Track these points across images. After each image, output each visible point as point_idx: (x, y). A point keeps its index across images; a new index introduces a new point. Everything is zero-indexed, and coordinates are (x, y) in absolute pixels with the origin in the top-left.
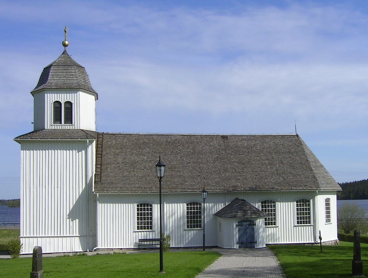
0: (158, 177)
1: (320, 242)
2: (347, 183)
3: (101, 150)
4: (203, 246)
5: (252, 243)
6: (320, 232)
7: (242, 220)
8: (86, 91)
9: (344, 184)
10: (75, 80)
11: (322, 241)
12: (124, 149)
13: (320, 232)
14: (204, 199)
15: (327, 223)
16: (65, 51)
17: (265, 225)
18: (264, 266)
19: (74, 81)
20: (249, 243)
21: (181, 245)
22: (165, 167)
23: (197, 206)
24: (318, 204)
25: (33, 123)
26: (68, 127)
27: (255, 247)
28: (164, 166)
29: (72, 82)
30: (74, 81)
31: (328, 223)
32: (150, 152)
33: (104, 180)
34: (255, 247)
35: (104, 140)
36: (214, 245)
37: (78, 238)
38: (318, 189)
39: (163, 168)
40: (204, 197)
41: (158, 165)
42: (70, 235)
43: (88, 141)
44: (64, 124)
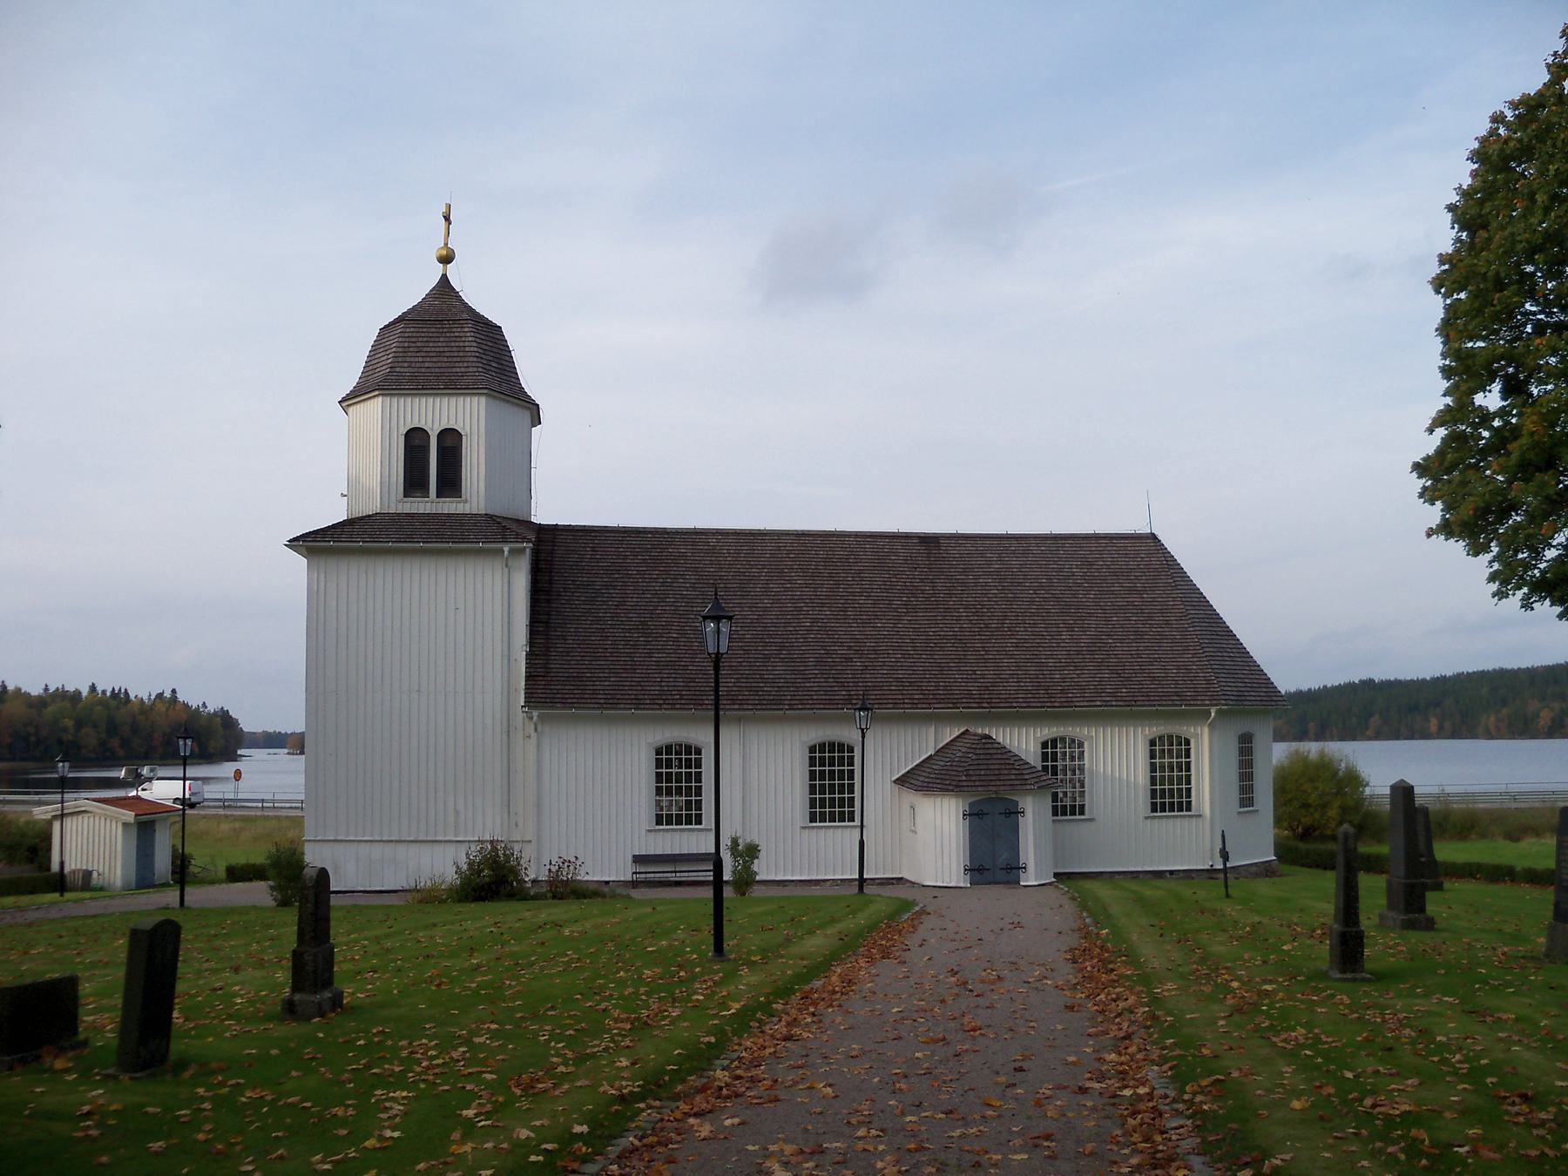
0: (708, 653)
1: (1221, 867)
2: (1301, 691)
3: (546, 578)
4: (857, 877)
5: (1012, 869)
6: (1223, 837)
7: (979, 798)
8: (503, 397)
9: (1290, 693)
10: (470, 364)
11: (1228, 865)
12: (617, 576)
13: (1223, 837)
14: (862, 730)
15: (1242, 810)
16: (444, 278)
17: (1053, 815)
18: (553, 574)
19: (467, 367)
20: (1001, 869)
21: (776, 875)
22: (733, 621)
23: (849, 768)
24: (964, 840)
25: (345, 496)
26: (449, 506)
27: (1022, 883)
28: (730, 618)
29: (463, 370)
30: (467, 367)
31: (1246, 809)
32: (696, 585)
33: (554, 670)
34: (1022, 883)
35: (556, 548)
36: (894, 876)
37: (713, 851)
38: (1216, 705)
39: (725, 627)
40: (864, 727)
41: (711, 614)
42: (429, 838)
43: (506, 549)
44: (437, 497)
